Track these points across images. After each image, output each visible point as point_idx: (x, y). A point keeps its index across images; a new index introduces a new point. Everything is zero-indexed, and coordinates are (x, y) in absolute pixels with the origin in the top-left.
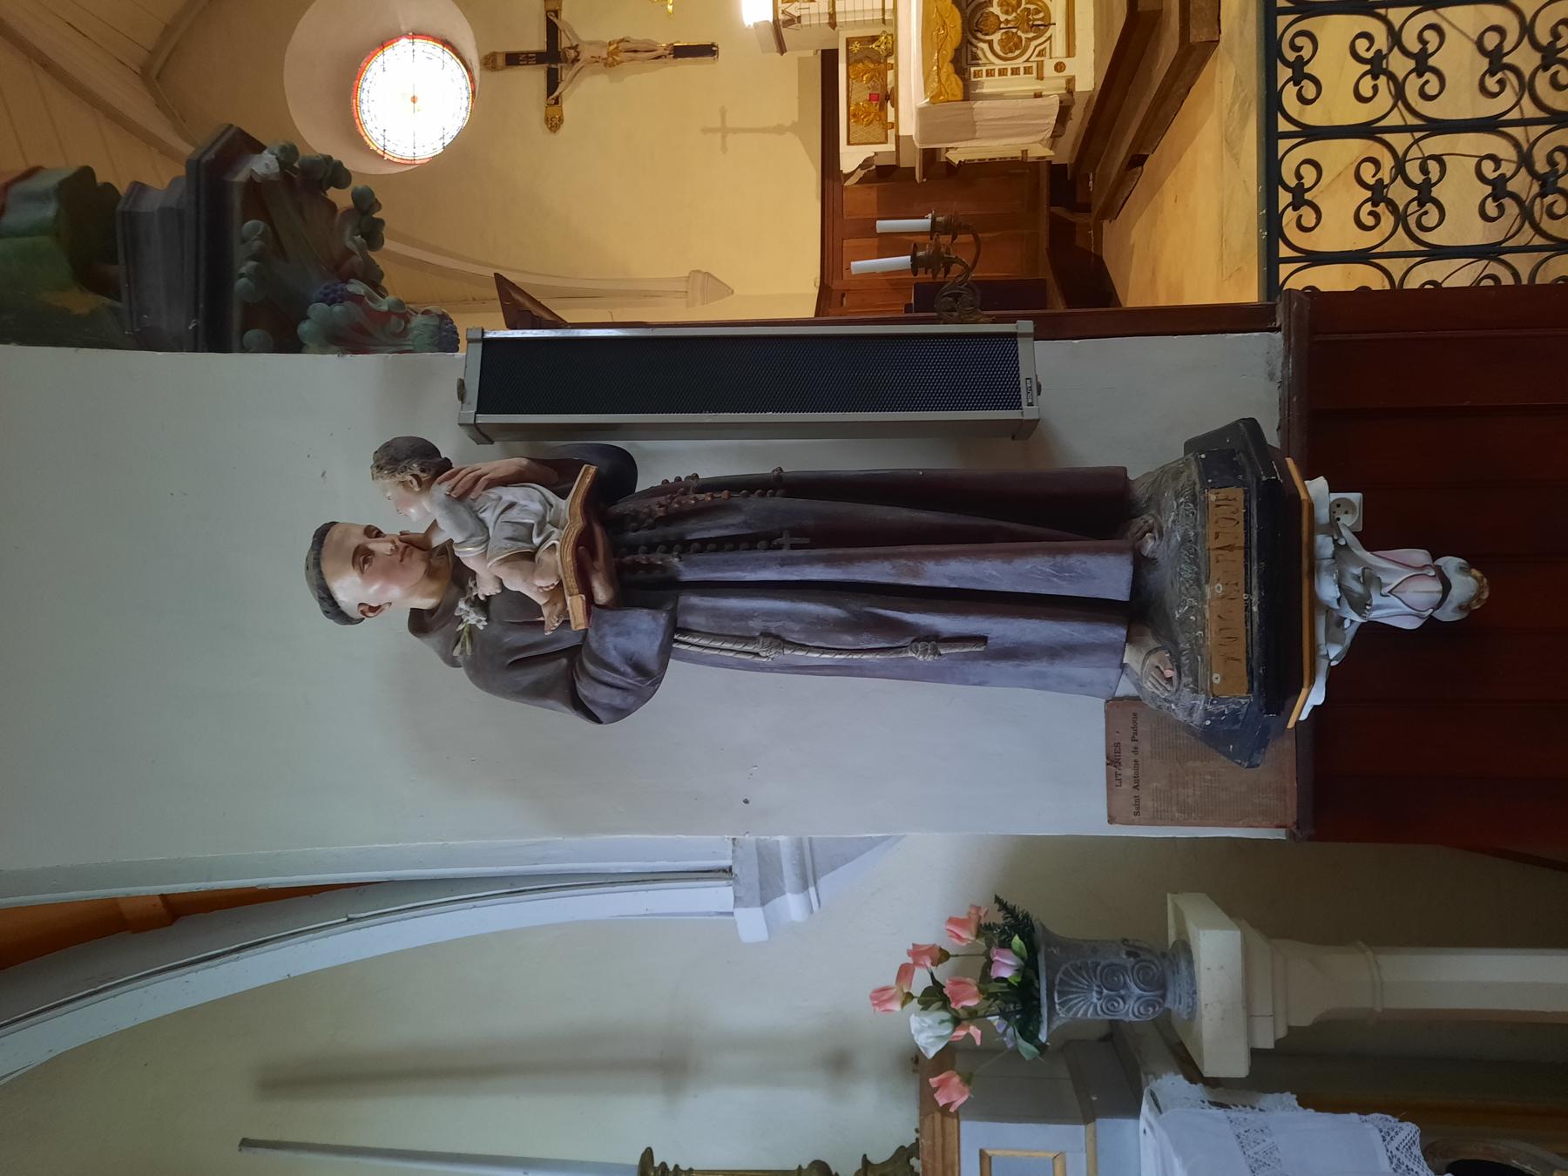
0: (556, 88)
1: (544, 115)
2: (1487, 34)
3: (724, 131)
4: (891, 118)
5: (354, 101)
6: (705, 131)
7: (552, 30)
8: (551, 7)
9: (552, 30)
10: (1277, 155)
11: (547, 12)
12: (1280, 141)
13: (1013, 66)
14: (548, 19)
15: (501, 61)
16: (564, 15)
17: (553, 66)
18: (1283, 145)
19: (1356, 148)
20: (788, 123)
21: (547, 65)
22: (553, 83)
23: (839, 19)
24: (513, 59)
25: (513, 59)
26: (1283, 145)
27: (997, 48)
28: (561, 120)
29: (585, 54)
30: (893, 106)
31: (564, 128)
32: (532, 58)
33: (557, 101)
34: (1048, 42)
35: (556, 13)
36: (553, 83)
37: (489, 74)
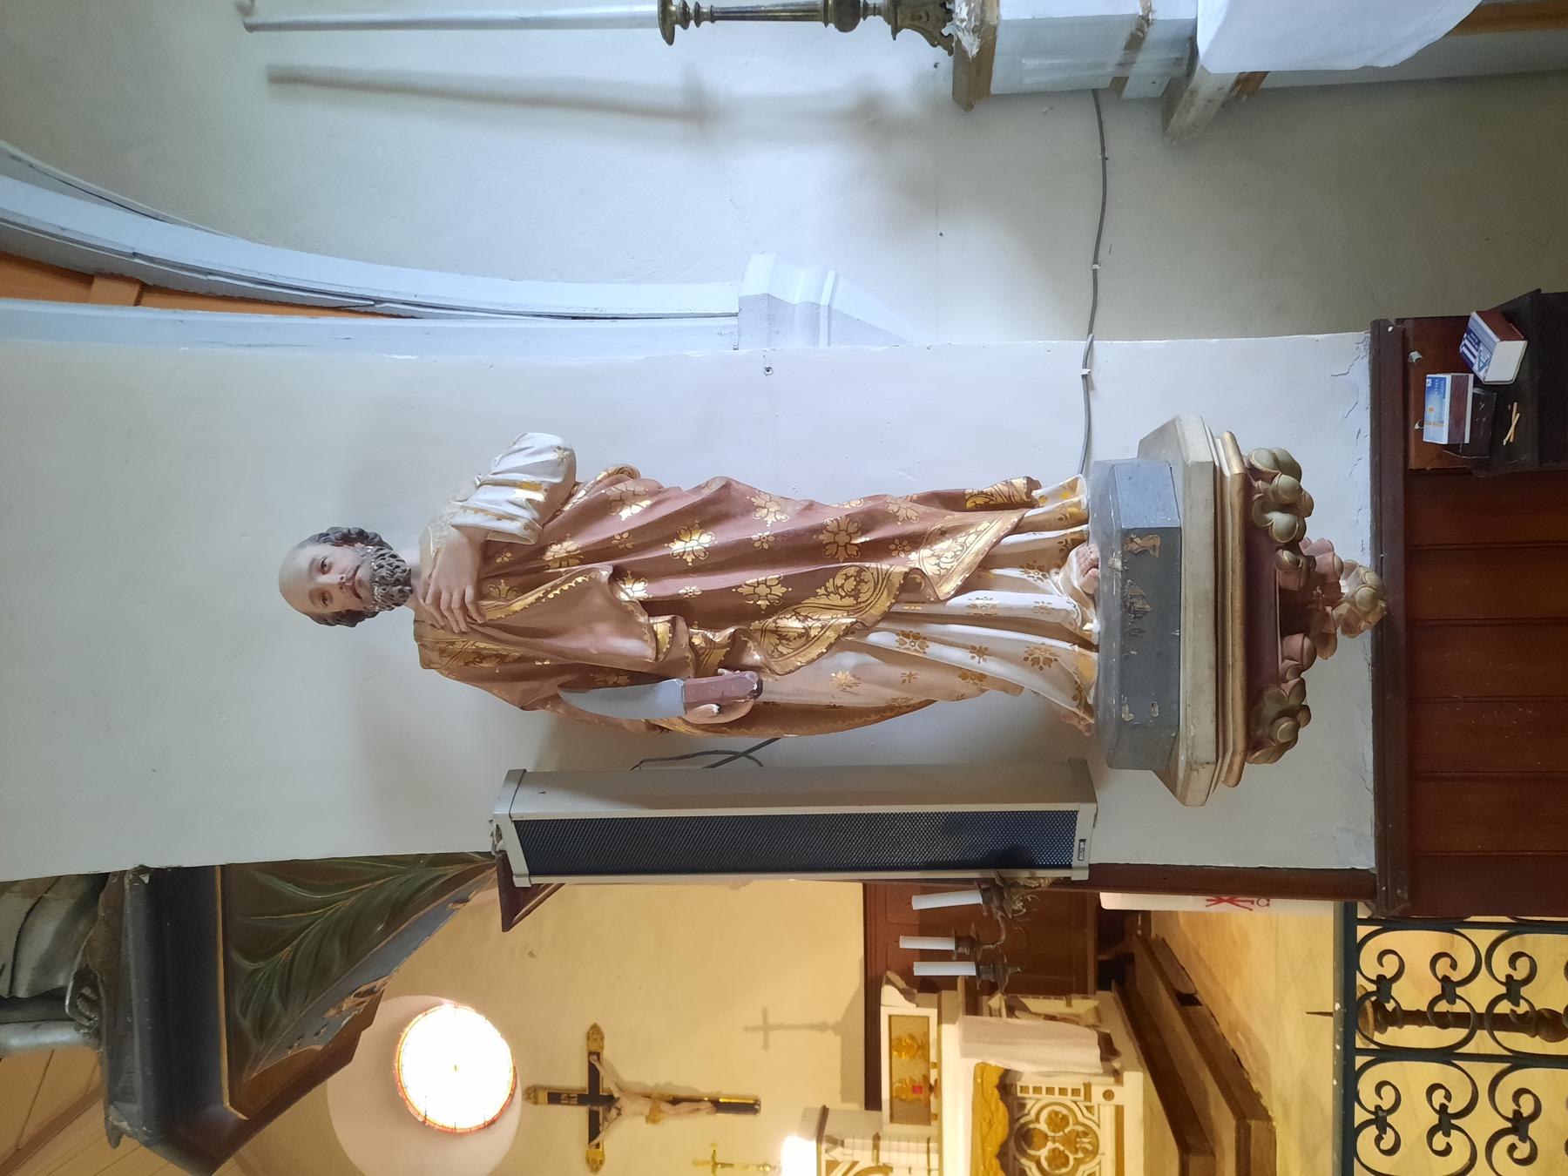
0: (596, 1137)
1: (585, 1156)
2: (1526, 959)
3: (766, 1028)
4: (933, 1058)
5: (396, 1064)
6: (747, 1029)
7: (594, 1074)
8: (594, 1048)
9: (594, 1074)
10: (1354, 1067)
11: (590, 1053)
12: (1359, 927)
13: (1052, 1096)
14: (590, 1063)
15: (543, 1096)
16: (606, 1054)
17: (595, 1108)
18: (1362, 931)
19: (1433, 1071)
20: (831, 1021)
21: (588, 1106)
22: (594, 1131)
23: (870, 1142)
24: (555, 1097)
25: (555, 1097)
26: (1362, 931)
27: (1045, 1164)
28: (601, 1163)
29: (625, 1103)
30: (936, 1097)
31: (604, 1169)
32: (574, 1097)
33: (598, 1146)
34: (1078, 1103)
35: (598, 1055)
36: (594, 1131)
37: (529, 1105)
